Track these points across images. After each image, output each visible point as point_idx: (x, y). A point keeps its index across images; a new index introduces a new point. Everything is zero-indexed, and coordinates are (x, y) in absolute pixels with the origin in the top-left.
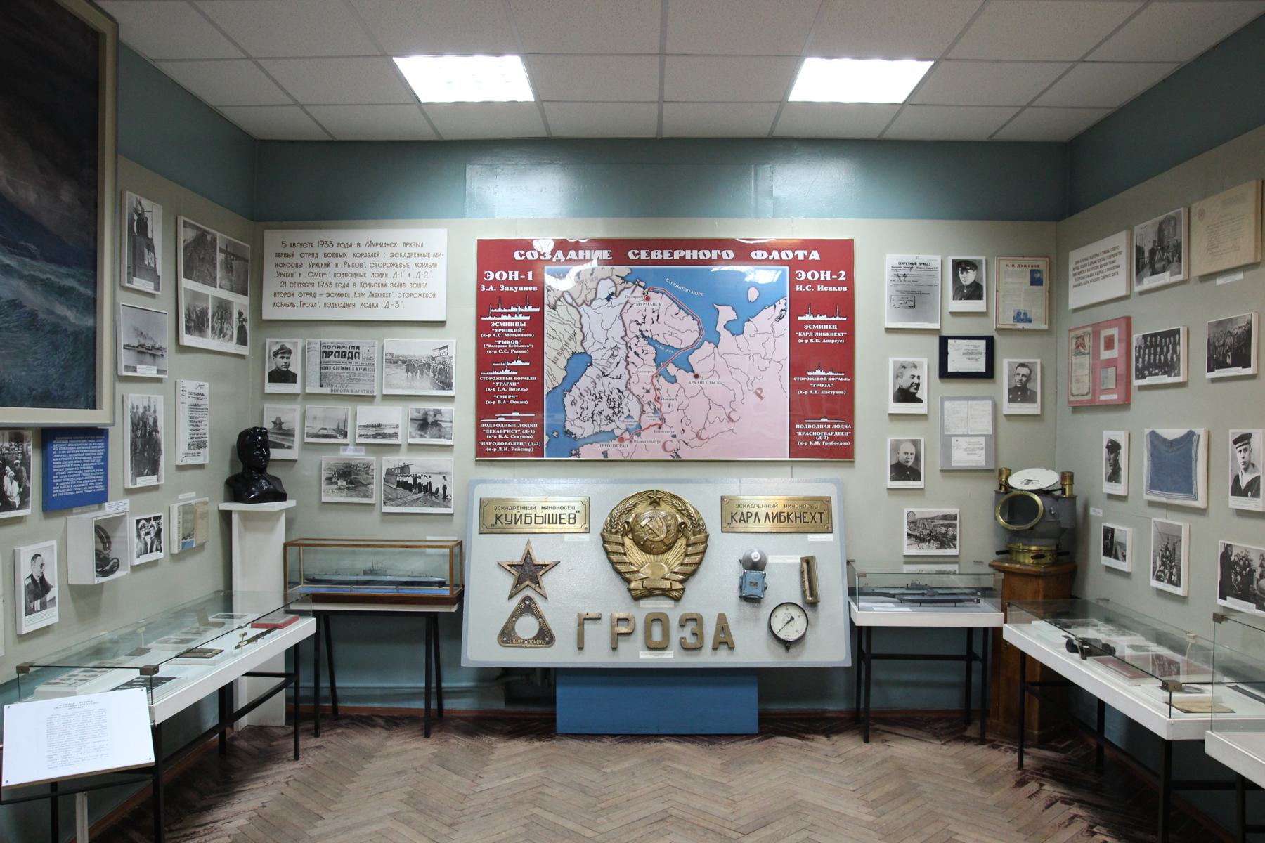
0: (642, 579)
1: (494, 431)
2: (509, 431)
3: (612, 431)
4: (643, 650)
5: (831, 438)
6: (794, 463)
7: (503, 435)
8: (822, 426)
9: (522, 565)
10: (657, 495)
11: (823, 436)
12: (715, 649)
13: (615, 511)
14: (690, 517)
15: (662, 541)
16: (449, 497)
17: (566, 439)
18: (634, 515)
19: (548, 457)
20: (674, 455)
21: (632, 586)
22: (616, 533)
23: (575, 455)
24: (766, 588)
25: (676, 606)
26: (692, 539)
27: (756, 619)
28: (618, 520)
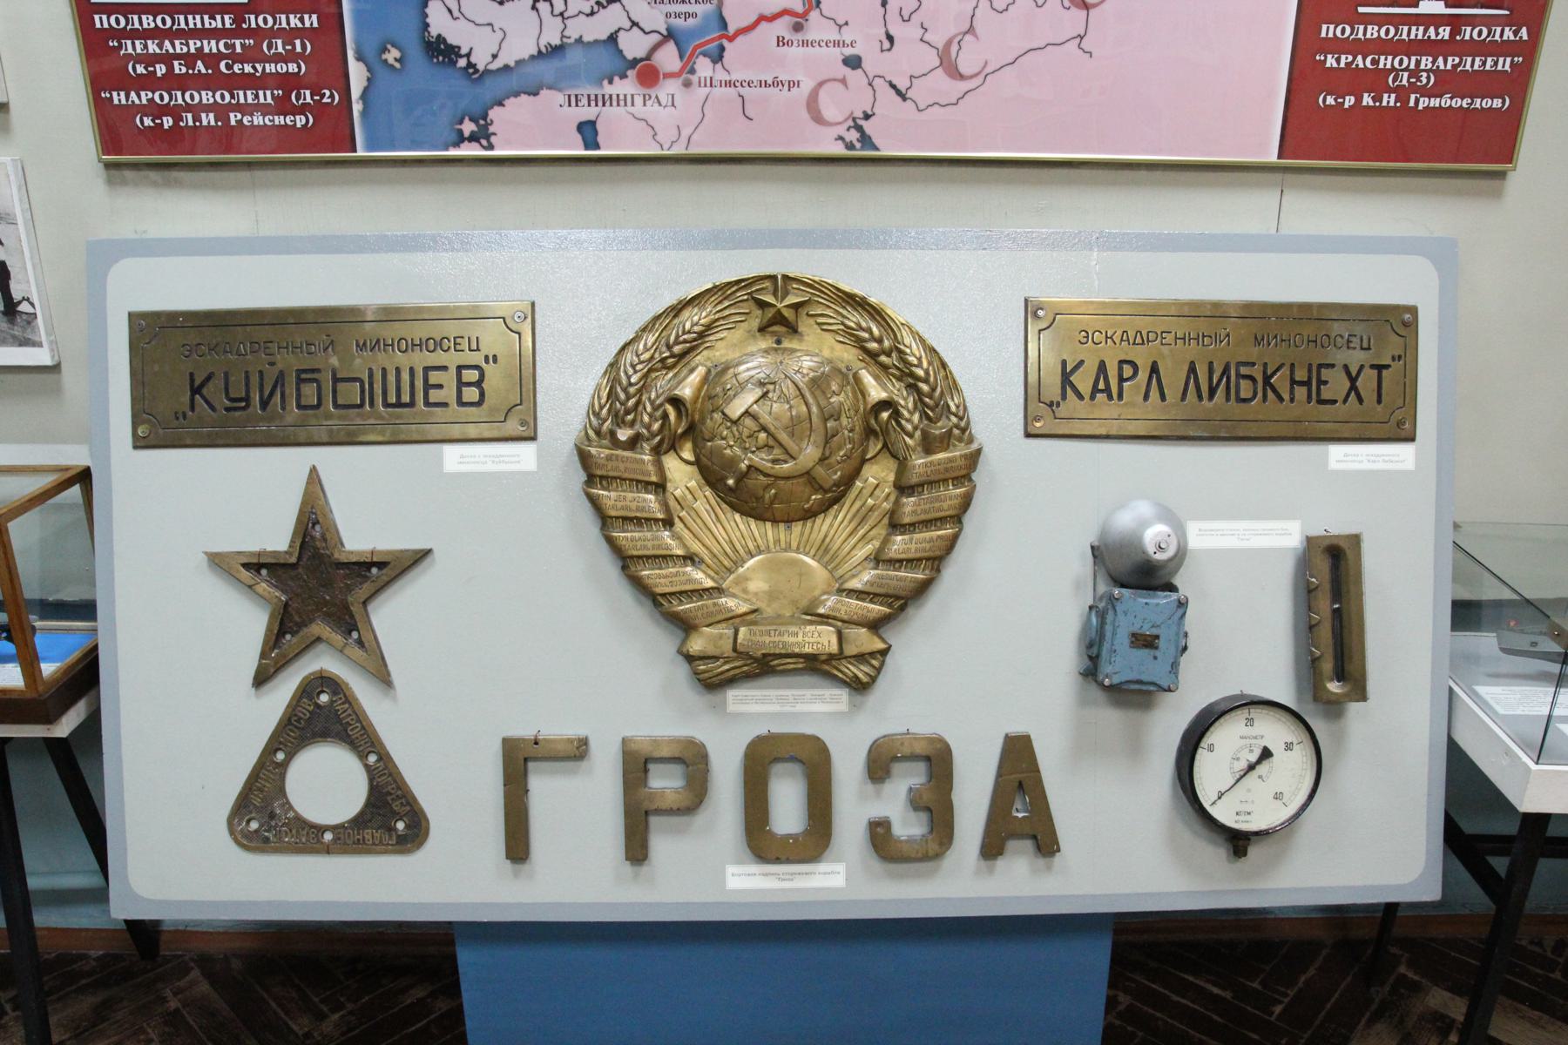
0: (733, 619)
1: (153, 47)
2: (210, 46)
3: (613, 39)
4: (739, 862)
5: (1446, 82)
6: (1289, 177)
7: (189, 60)
8: (1418, 33)
9: (293, 566)
10: (786, 294)
11: (1415, 73)
12: (992, 849)
13: (629, 357)
14: (907, 377)
15: (808, 474)
16: (24, 307)
17: (445, 83)
18: (701, 370)
19: (370, 148)
20: (853, 136)
21: (696, 645)
22: (633, 443)
23: (473, 138)
24: (1185, 648)
25: (855, 707)
26: (919, 462)
27: (1135, 748)
28: (640, 391)
